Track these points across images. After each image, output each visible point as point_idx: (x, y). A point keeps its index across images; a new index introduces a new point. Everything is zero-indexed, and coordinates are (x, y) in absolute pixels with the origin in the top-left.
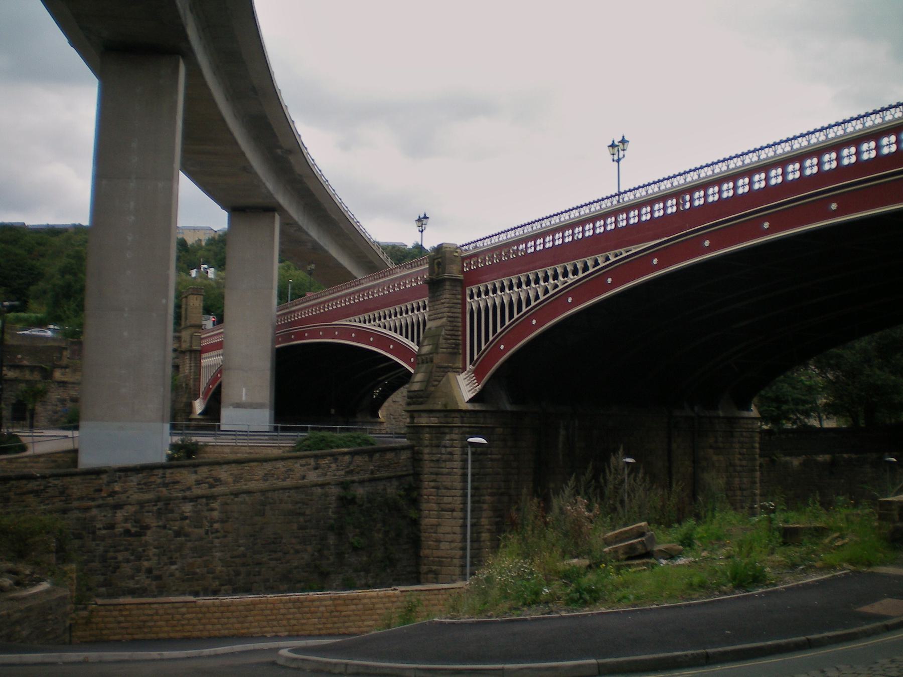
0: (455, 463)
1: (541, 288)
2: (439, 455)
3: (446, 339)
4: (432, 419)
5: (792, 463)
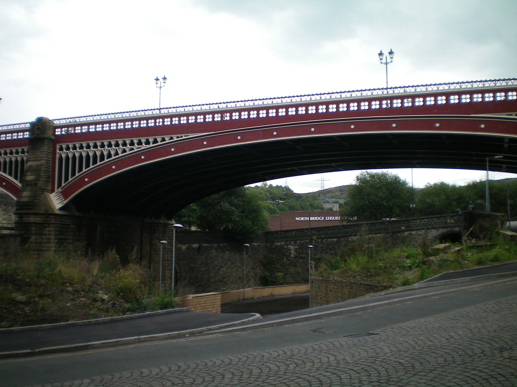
0: (51, 244)
1: (120, 150)
2: (41, 240)
3: (45, 173)
4: (38, 219)
5: (182, 248)
